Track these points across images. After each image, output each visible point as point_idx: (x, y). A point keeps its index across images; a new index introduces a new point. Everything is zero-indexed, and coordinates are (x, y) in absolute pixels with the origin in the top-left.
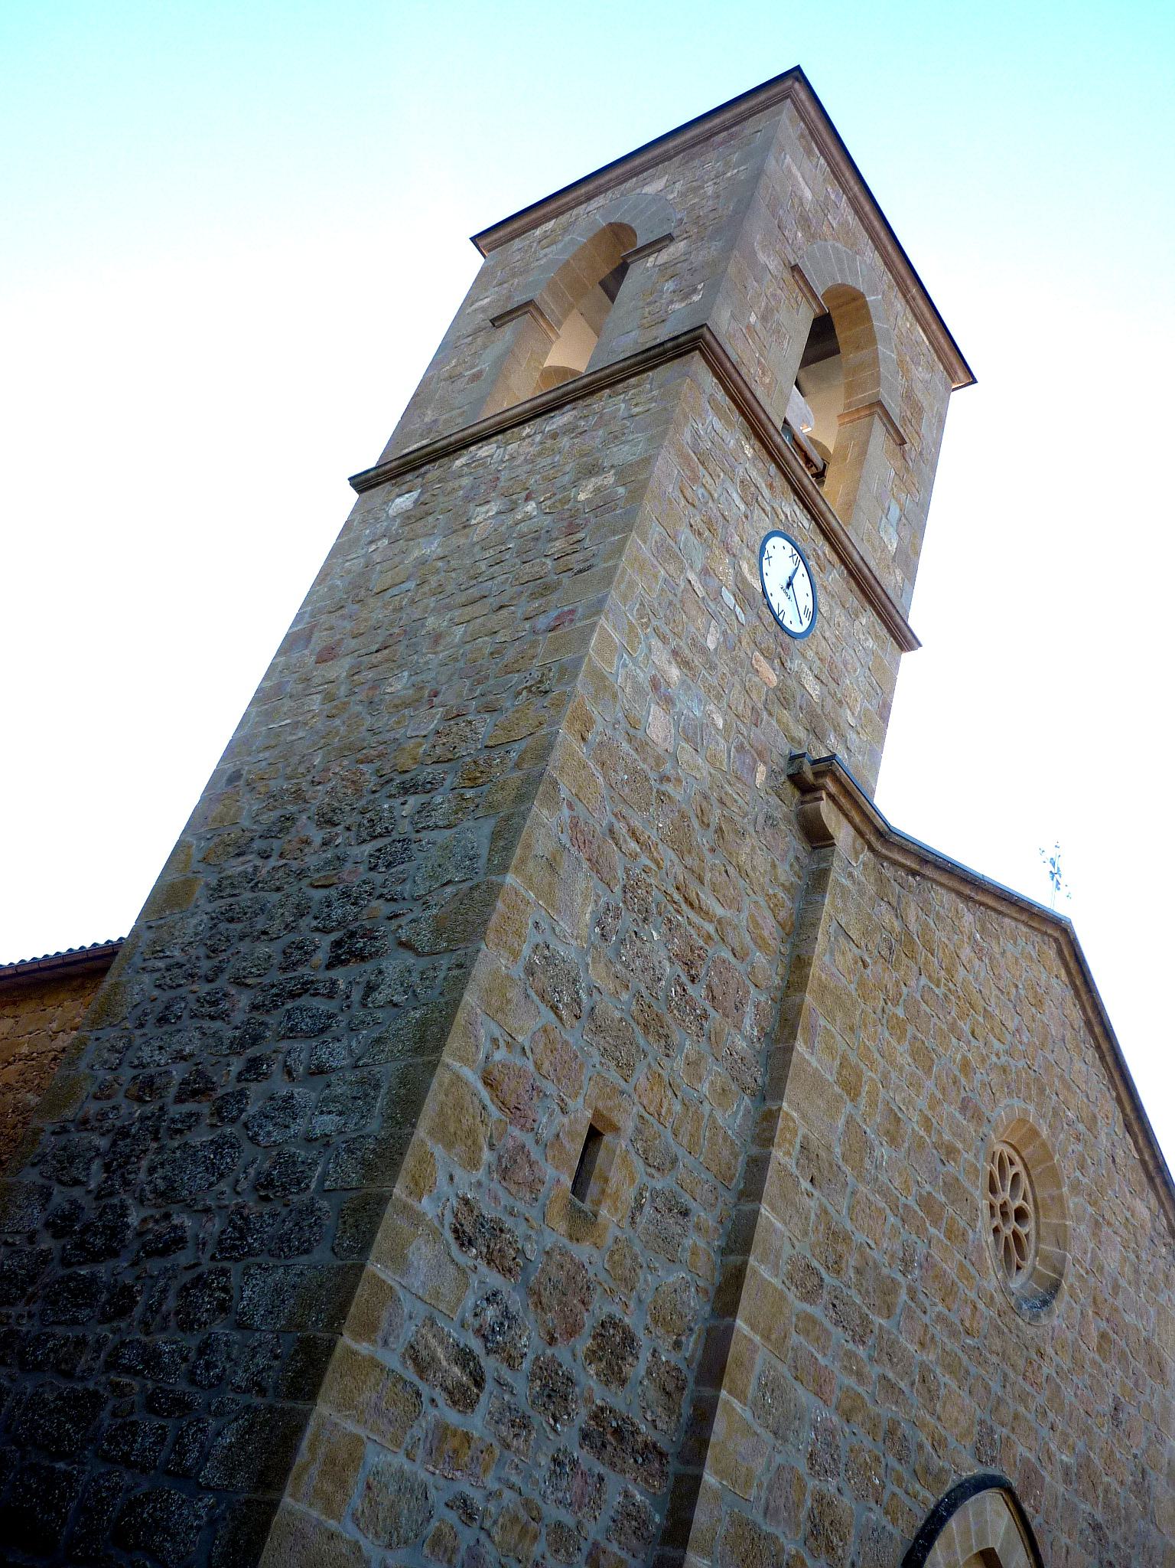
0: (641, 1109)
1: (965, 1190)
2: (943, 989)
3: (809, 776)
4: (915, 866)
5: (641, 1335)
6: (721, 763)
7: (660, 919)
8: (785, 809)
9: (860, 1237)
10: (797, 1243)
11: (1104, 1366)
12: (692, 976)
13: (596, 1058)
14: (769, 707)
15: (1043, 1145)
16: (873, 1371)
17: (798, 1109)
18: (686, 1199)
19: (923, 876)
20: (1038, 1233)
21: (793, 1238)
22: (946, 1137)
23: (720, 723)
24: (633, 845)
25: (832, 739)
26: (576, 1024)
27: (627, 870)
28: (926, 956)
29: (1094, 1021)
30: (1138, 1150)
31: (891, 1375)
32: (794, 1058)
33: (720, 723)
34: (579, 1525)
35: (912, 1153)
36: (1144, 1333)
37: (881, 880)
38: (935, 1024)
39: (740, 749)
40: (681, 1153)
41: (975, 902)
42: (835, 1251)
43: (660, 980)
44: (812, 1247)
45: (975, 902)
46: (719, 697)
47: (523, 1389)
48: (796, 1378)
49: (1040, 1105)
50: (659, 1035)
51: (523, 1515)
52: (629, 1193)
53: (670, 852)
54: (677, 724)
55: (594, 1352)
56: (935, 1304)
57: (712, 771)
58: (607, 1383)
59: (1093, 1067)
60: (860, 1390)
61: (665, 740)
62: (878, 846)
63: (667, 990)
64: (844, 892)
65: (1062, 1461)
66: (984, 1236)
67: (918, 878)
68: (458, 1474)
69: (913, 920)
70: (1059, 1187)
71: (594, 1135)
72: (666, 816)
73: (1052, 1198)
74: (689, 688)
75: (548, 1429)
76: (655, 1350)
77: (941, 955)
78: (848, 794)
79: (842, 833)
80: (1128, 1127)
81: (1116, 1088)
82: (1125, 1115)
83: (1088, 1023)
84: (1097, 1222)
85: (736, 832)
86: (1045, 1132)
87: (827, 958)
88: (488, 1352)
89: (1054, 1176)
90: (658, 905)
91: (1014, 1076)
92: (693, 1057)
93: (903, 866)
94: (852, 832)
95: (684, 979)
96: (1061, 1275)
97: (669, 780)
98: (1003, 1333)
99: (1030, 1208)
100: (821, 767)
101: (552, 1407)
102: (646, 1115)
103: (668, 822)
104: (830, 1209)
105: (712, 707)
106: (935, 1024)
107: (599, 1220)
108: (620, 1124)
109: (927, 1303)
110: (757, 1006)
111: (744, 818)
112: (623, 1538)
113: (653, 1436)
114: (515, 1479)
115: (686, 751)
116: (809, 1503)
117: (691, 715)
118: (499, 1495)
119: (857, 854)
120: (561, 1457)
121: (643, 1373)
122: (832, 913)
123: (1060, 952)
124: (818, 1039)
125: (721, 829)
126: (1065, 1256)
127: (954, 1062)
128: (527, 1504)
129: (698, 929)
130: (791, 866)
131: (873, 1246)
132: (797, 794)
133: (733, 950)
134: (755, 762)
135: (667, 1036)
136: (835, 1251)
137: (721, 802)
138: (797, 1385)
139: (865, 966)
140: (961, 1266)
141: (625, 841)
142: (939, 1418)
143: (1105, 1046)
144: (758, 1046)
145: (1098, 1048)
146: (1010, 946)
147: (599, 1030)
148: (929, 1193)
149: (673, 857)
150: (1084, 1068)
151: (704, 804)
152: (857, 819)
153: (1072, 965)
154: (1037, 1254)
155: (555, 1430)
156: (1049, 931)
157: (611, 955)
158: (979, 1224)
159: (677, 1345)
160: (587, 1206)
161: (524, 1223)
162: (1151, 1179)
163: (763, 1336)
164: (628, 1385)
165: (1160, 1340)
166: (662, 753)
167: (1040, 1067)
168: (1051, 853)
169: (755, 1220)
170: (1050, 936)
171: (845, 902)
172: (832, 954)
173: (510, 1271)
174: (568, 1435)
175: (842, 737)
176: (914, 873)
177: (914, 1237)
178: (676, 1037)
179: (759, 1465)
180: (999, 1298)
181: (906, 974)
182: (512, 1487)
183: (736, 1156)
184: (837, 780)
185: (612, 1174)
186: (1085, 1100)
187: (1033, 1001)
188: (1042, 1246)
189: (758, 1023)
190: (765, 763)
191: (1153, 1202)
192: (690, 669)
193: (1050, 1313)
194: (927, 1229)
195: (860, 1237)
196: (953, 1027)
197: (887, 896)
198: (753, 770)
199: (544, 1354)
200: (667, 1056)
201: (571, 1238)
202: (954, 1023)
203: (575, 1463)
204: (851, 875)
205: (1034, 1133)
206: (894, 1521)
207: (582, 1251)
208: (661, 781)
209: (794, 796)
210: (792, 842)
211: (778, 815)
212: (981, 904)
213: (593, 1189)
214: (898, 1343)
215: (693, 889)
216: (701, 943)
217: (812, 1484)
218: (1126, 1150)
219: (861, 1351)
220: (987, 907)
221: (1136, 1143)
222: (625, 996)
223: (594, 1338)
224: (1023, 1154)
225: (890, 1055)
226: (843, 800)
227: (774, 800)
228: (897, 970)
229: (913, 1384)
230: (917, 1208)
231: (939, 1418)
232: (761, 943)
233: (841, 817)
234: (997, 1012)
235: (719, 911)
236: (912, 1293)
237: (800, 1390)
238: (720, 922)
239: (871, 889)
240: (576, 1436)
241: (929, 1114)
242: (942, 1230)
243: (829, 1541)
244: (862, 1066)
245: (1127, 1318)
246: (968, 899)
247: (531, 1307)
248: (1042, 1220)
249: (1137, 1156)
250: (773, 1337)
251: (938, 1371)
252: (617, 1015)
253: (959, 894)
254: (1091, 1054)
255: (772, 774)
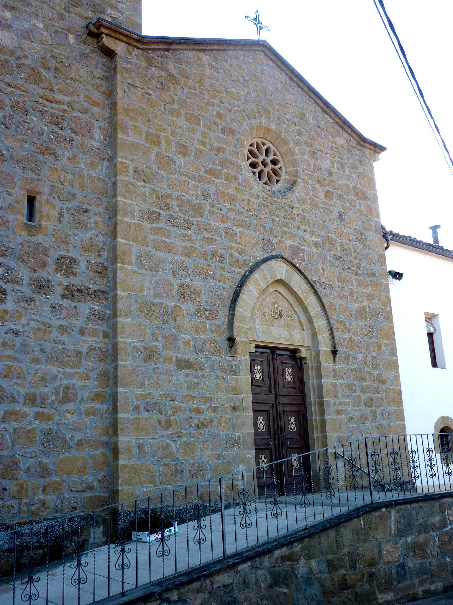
0: (51, 183)
1: (232, 161)
2: (198, 90)
3: (94, 30)
4: (166, 47)
5: (79, 257)
6: (47, 42)
7: (35, 112)
8: (91, 48)
9: (175, 194)
10: (141, 205)
11: (330, 203)
12: (60, 128)
13: (20, 172)
14: (68, 10)
15: (275, 132)
16: (199, 237)
17: (126, 158)
18: (85, 206)
19: (173, 50)
20: (285, 164)
21: (139, 204)
22: (215, 145)
23: (41, 26)
24: (10, 89)
25: (109, 11)
26: (5, 163)
27: (11, 99)
28: (184, 81)
29: (292, 76)
30: (333, 119)
31: (208, 236)
32: (119, 141)
33: (41, 26)
34: (71, 324)
35: (197, 157)
36: (351, 185)
37: (148, 59)
38: (197, 105)
39: (56, 32)
40: (76, 192)
41: (209, 50)
42: (165, 202)
43: (43, 134)
44: (151, 204)
45: (209, 50)
46: (36, 16)
47: (26, 290)
48: (157, 250)
49: (268, 118)
50: (51, 154)
51: (42, 327)
52: (55, 213)
53: (31, 85)
54: (17, 35)
55: (57, 269)
56: (226, 206)
57: (44, 46)
58: (67, 277)
59: (298, 94)
60: (193, 245)
61: (12, 43)
62: (140, 46)
63: (48, 136)
64: (127, 70)
65: (313, 241)
66: (247, 175)
67: (170, 51)
68: (6, 323)
69: (172, 69)
70: (288, 145)
71: (31, 200)
72: (23, 72)
73: (287, 151)
74: (18, 17)
75: (43, 299)
76: (87, 261)
77: (193, 77)
78: (114, 31)
79: (119, 47)
80: (325, 112)
81: (313, 99)
82: (321, 108)
83: (290, 78)
84: (313, 153)
85: (66, 66)
86: (273, 127)
87: (126, 99)
88: (5, 283)
89: (285, 142)
90: (32, 107)
91: (250, 111)
92: (71, 156)
93: (160, 49)
94: (125, 45)
95: (56, 129)
96: (297, 177)
97: (20, 58)
98: (267, 206)
99: (279, 158)
100: (97, 25)
101: (43, 292)
102: (54, 184)
103: (25, 74)
104: (156, 188)
105: (34, 21)
106: (197, 105)
107: (42, 226)
108: (41, 191)
109: (220, 206)
110: (100, 128)
111: (68, 59)
112: (94, 322)
113: (97, 288)
114: (33, 317)
115: (26, 44)
116: (177, 288)
117: (24, 28)
118: (28, 324)
119: (131, 53)
120: (54, 306)
121: (85, 269)
122: (123, 80)
123: (266, 55)
124: (130, 130)
125: (58, 68)
126: (297, 170)
127: (213, 116)
128: (43, 323)
129: (58, 109)
130: (102, 69)
131: (185, 194)
132: (95, 40)
133: (80, 111)
134: (67, 35)
135: (54, 153)
136: (165, 202)
137: (54, 57)
138: (159, 252)
139: (150, 95)
140: (237, 189)
141: (5, 89)
142: (239, 244)
143: (301, 85)
144: (105, 142)
145: (299, 86)
146: (235, 61)
147: (18, 161)
148: (211, 168)
149: (34, 86)
150: (292, 97)
151: (44, 61)
152: (124, 39)
153: (273, 58)
154: (286, 172)
155: (48, 298)
156: (256, 49)
157: (14, 133)
158: (243, 171)
159: (99, 256)
160: (36, 224)
161: (6, 238)
162: (343, 128)
163: (133, 241)
164: (77, 275)
165: (361, 185)
166: (13, 49)
167: (265, 103)
168: (253, 16)
169: (117, 203)
170: (258, 50)
171: (129, 74)
172: (128, 96)
173: (5, 255)
174: (55, 298)
175: (116, 8)
176: (168, 50)
177: (208, 186)
178: (59, 152)
179: (146, 283)
180: (262, 195)
181: (174, 91)
182: (33, 320)
183: (107, 184)
184: (106, 27)
185: (43, 209)
186: (296, 109)
187: (254, 79)
188: (287, 169)
189: (102, 134)
190: (72, 33)
191: (346, 136)
192: (16, 10)
193: (293, 192)
194: (214, 181)
195: (175, 194)
196: (208, 103)
197: (154, 64)
198: (67, 38)
199: (33, 276)
200: (57, 160)
201: (30, 236)
202: (208, 101)
203: (60, 306)
204: (130, 62)
205: (269, 130)
206: (224, 283)
207: (39, 238)
208: (17, 59)
209: (93, 41)
210: (100, 60)
211: (88, 52)
212: (212, 50)
213: (37, 216)
214: (209, 224)
215: (50, 95)
216: (61, 114)
217: (176, 282)
218: (326, 120)
219: (189, 232)
220: (216, 50)
221: (330, 117)
222: (27, 146)
223: (56, 264)
224: (268, 139)
225: (174, 124)
226: (113, 34)
227: (83, 46)
228: (169, 91)
229: (221, 236)
230: (207, 175)
231: (239, 244)
232: (94, 104)
233: (116, 41)
234: (233, 90)
235: (67, 99)
236: (212, 205)
237: (160, 254)
238: (68, 103)
239: (144, 64)
240: (59, 298)
241: (203, 139)
242: (223, 179)
243: (191, 297)
244: (158, 133)
245: (340, 183)
246: (204, 50)
247: (21, 263)
248: (285, 160)
249: (332, 121)
250: (139, 240)
251: (234, 228)
252: (25, 153)
253: (197, 50)
254: (295, 90)
255: (78, 36)
